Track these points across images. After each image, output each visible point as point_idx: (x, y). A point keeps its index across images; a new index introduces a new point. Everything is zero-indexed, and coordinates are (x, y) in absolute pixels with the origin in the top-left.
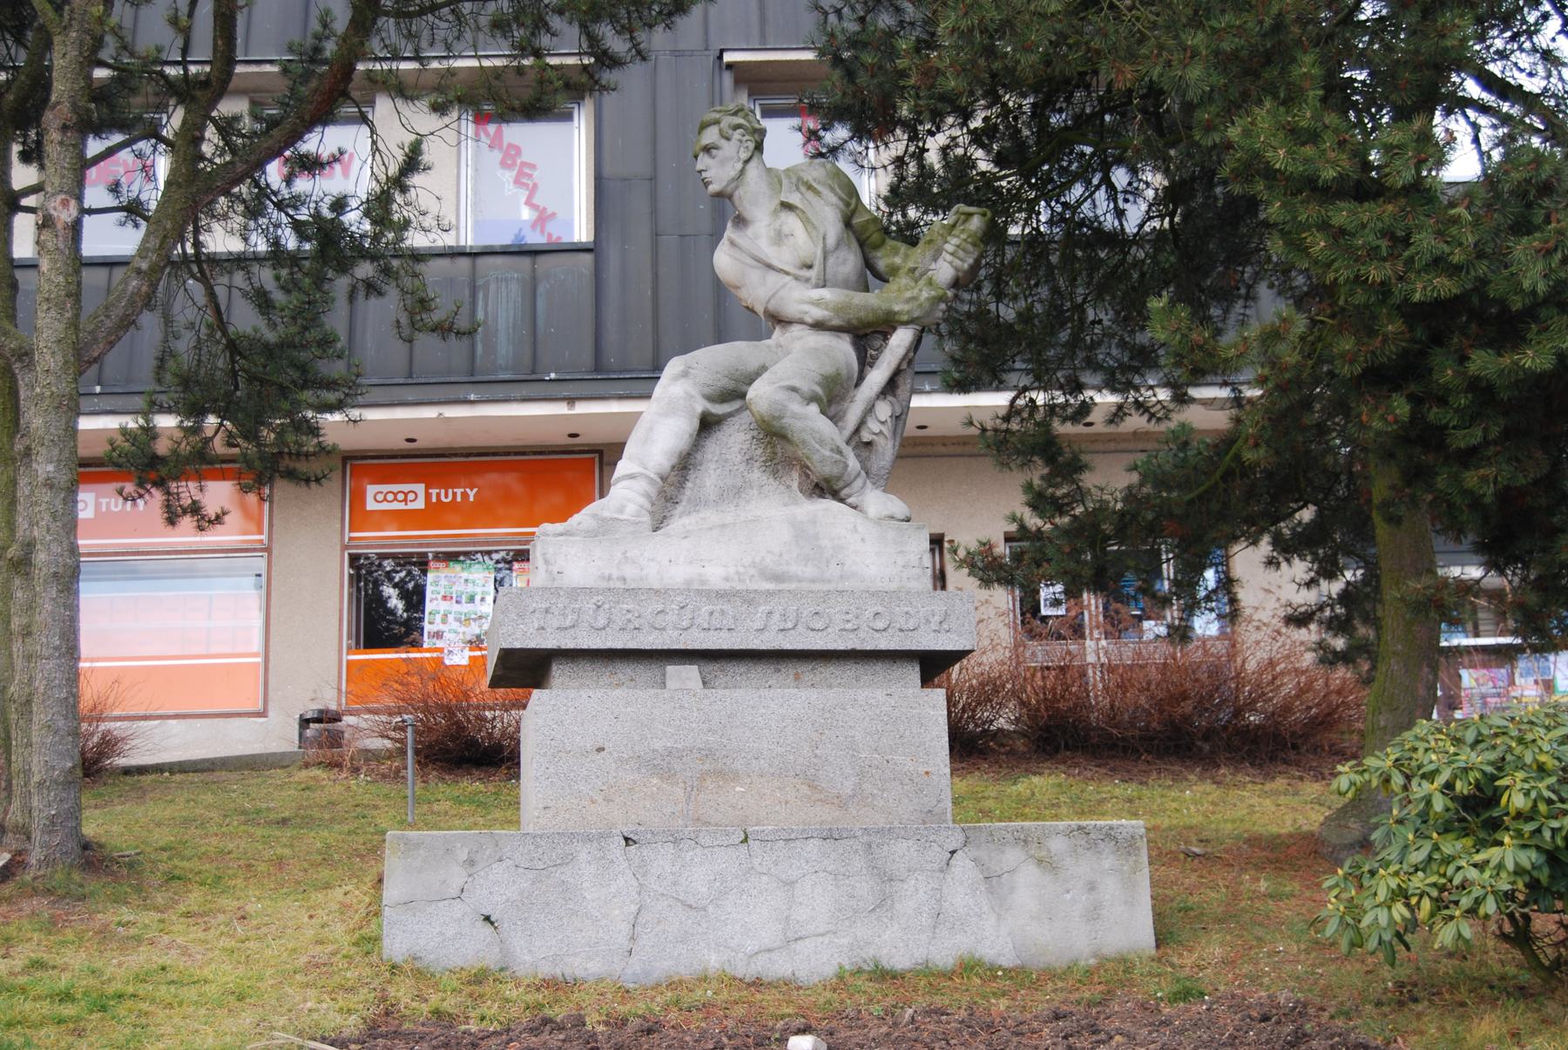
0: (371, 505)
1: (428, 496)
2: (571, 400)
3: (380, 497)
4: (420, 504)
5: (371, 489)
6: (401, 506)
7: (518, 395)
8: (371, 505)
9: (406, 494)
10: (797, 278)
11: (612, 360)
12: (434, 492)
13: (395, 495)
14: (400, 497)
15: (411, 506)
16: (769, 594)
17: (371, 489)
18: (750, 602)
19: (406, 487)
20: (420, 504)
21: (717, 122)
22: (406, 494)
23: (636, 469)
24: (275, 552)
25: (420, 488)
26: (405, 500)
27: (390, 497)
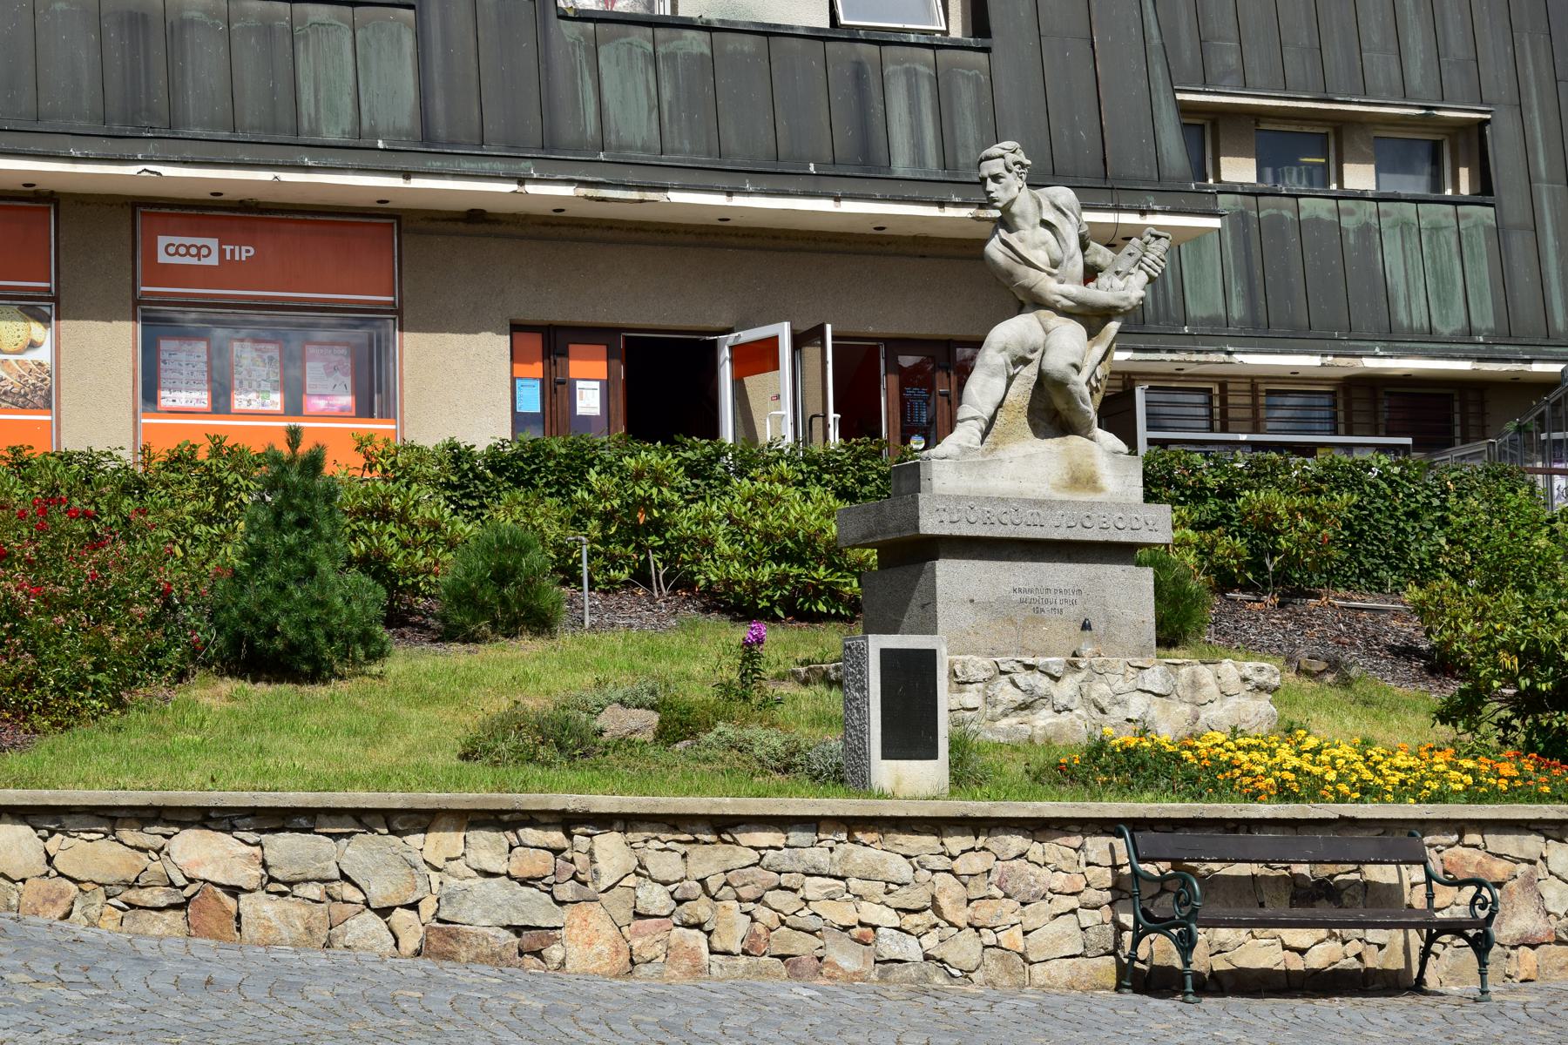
0: (163, 258)
1: (222, 253)
2: (407, 175)
3: (172, 250)
4: (213, 260)
5: (163, 241)
6: (194, 261)
7: (356, 164)
8: (163, 258)
9: (199, 249)
10: (1050, 274)
11: (441, 131)
12: (228, 248)
13: (188, 248)
14: (193, 251)
15: (204, 262)
16: (1062, 503)
17: (163, 241)
18: (1051, 508)
19: (199, 241)
20: (213, 260)
21: (1002, 157)
22: (199, 249)
23: (976, 413)
24: (63, 302)
25: (213, 243)
26: (198, 255)
27: (182, 250)
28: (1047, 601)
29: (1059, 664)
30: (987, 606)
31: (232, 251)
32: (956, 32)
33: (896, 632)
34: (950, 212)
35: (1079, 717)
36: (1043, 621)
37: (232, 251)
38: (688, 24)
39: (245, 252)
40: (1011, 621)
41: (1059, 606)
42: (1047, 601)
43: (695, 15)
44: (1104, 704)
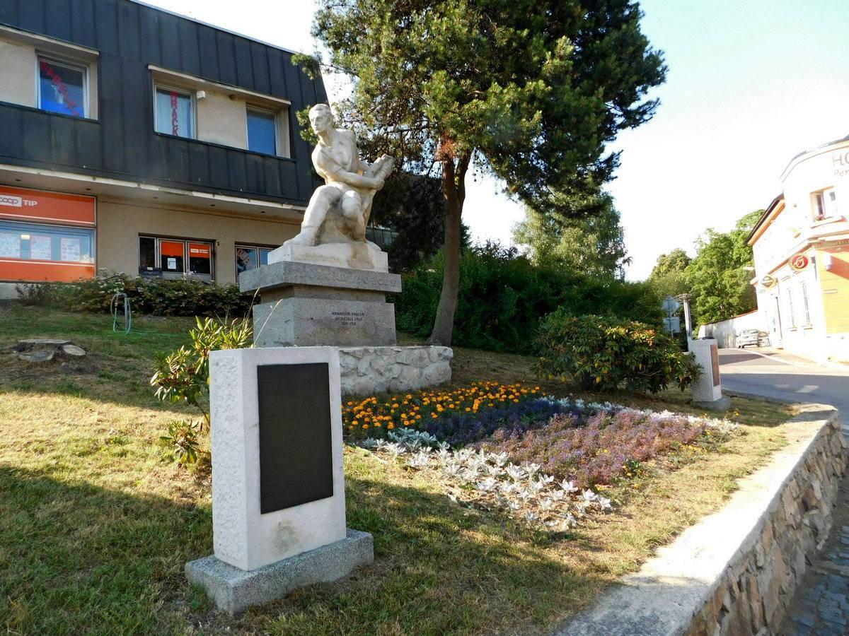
1: (23, 203)
9: (13, 200)
12: (26, 201)
20: (19, 205)
28: (348, 319)
29: (360, 351)
30: (319, 322)
31: (28, 203)
32: (288, 156)
33: (41, 77)
34: (285, 207)
35: (371, 378)
36: (347, 329)
37: (28, 203)
38: (201, 143)
39: (33, 203)
40: (331, 329)
41: (354, 321)
42: (348, 319)
43: (203, 140)
44: (382, 371)
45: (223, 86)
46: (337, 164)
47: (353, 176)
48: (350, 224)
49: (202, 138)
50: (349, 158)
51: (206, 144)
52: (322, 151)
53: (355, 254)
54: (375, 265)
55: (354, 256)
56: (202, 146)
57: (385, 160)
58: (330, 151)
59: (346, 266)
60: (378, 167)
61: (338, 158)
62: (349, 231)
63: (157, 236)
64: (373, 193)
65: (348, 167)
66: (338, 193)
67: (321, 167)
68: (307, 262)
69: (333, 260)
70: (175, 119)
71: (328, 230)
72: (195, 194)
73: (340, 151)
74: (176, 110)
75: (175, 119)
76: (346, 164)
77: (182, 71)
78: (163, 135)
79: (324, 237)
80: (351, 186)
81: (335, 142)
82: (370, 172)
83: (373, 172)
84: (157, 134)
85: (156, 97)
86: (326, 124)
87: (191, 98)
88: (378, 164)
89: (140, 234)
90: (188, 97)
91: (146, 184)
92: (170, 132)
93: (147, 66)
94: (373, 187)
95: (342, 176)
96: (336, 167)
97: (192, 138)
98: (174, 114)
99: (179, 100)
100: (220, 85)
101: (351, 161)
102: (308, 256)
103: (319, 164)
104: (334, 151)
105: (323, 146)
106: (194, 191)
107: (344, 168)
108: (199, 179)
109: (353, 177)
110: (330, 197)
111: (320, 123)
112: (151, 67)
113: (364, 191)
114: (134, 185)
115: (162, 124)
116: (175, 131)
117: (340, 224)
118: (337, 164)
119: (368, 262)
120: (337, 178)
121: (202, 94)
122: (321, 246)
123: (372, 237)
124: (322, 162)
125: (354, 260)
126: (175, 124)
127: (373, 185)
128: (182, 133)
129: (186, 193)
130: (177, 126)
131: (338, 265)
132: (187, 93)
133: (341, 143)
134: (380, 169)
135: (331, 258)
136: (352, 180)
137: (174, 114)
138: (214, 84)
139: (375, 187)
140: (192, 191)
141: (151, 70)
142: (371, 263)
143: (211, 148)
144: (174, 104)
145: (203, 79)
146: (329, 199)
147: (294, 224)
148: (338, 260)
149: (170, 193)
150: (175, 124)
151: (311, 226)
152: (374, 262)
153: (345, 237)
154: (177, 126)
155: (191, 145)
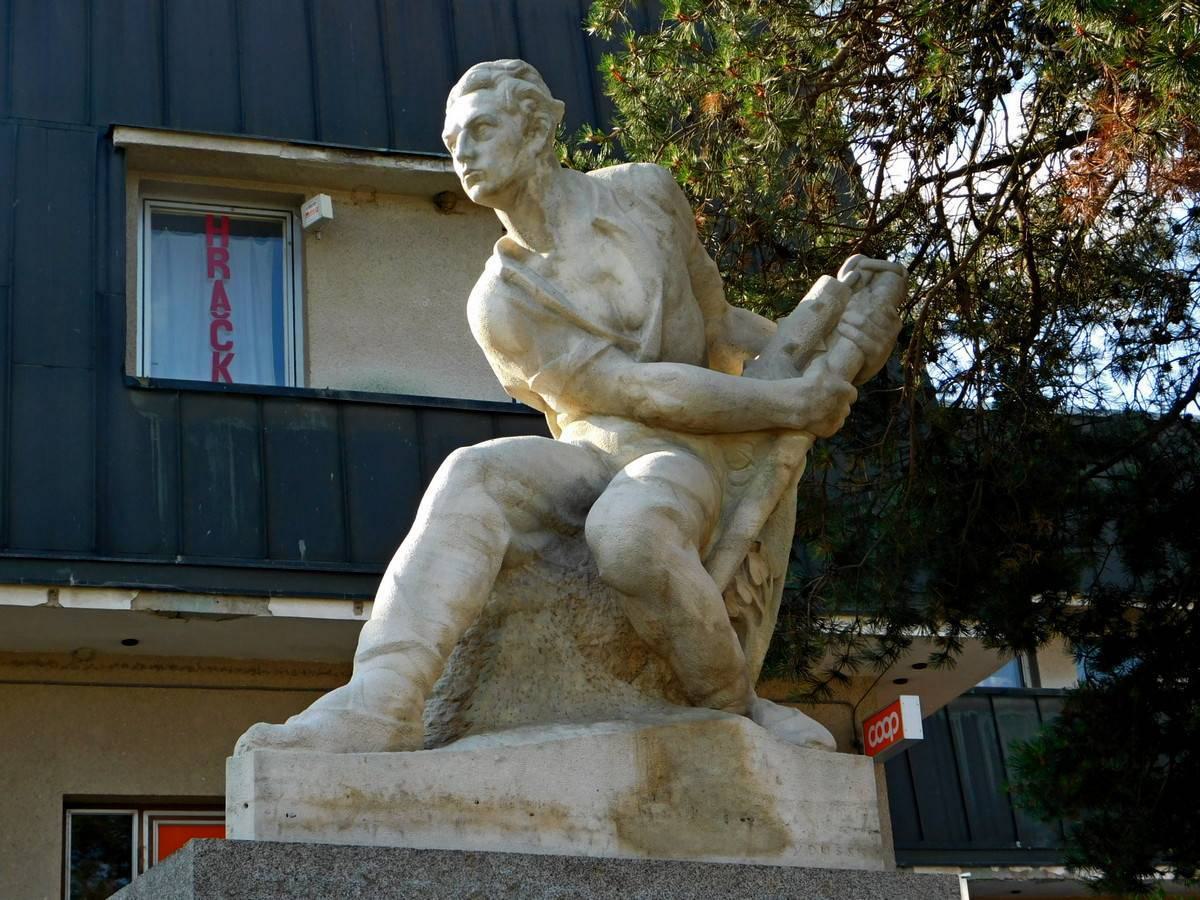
38: (308, 397)
45: (404, 164)
46: (588, 330)
47: (663, 381)
48: (646, 619)
49: (324, 379)
50: (648, 297)
51: (335, 401)
52: (506, 278)
53: (665, 778)
54: (797, 832)
55: (660, 781)
56: (314, 409)
57: (854, 285)
58: (550, 273)
59: (603, 845)
60: (814, 321)
61: (588, 304)
62: (650, 660)
63: (143, 804)
64: (793, 452)
65: (646, 338)
66: (589, 470)
67: (509, 355)
68: (356, 837)
69: (518, 818)
70: (221, 322)
71: (516, 658)
72: (281, 608)
73: (602, 263)
74: (228, 288)
75: (221, 322)
76: (636, 327)
77: (240, 131)
78: (160, 388)
79: (481, 709)
80: (658, 425)
81: (573, 227)
82: (775, 353)
83: (791, 349)
84: (135, 385)
85: (143, 244)
86: (518, 146)
87: (287, 229)
88: (817, 306)
89: (69, 802)
90: (268, 230)
91: (82, 586)
92: (200, 371)
93: (110, 136)
94: (780, 419)
95: (613, 385)
96: (576, 347)
97: (289, 383)
98: (220, 298)
99: (241, 249)
100: (390, 163)
101: (657, 304)
102: (358, 801)
103: (496, 344)
104: (566, 271)
105: (512, 255)
106: (276, 595)
107: (626, 348)
108: (302, 547)
109: (668, 384)
110: (515, 486)
111: (483, 147)
112: (121, 137)
113: (744, 449)
114: (35, 598)
115: (164, 341)
116: (220, 367)
117: (599, 627)
118: (588, 330)
119: (747, 819)
120: (592, 409)
121: (320, 207)
122: (472, 744)
123: (792, 668)
124: (508, 337)
125: (657, 808)
126: (222, 340)
127: (787, 411)
128: (250, 371)
129: (244, 607)
130: (229, 345)
131: (552, 843)
132: (263, 217)
133: (600, 228)
134: (828, 332)
135: (508, 806)
136: (661, 399)
137: (220, 298)
138: (367, 162)
139: (793, 420)
140: (265, 596)
141: (122, 149)
142: (767, 822)
143: (350, 411)
144: (217, 262)
145: (323, 148)
146: (513, 501)
147: (327, 663)
148: (557, 814)
149: (179, 615)
150: (222, 340)
151: (398, 647)
152: (786, 814)
153: (628, 694)
154: (229, 345)
155: (271, 408)
